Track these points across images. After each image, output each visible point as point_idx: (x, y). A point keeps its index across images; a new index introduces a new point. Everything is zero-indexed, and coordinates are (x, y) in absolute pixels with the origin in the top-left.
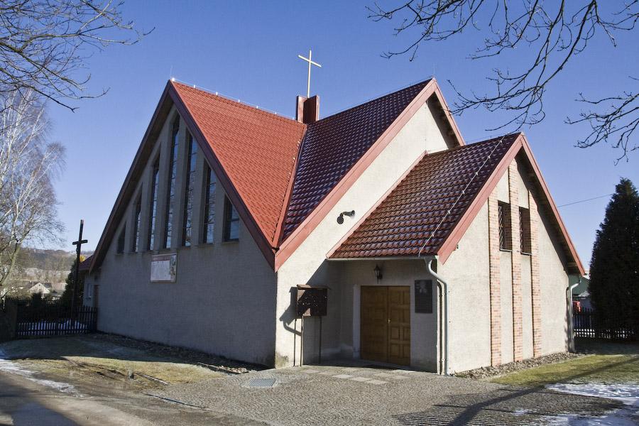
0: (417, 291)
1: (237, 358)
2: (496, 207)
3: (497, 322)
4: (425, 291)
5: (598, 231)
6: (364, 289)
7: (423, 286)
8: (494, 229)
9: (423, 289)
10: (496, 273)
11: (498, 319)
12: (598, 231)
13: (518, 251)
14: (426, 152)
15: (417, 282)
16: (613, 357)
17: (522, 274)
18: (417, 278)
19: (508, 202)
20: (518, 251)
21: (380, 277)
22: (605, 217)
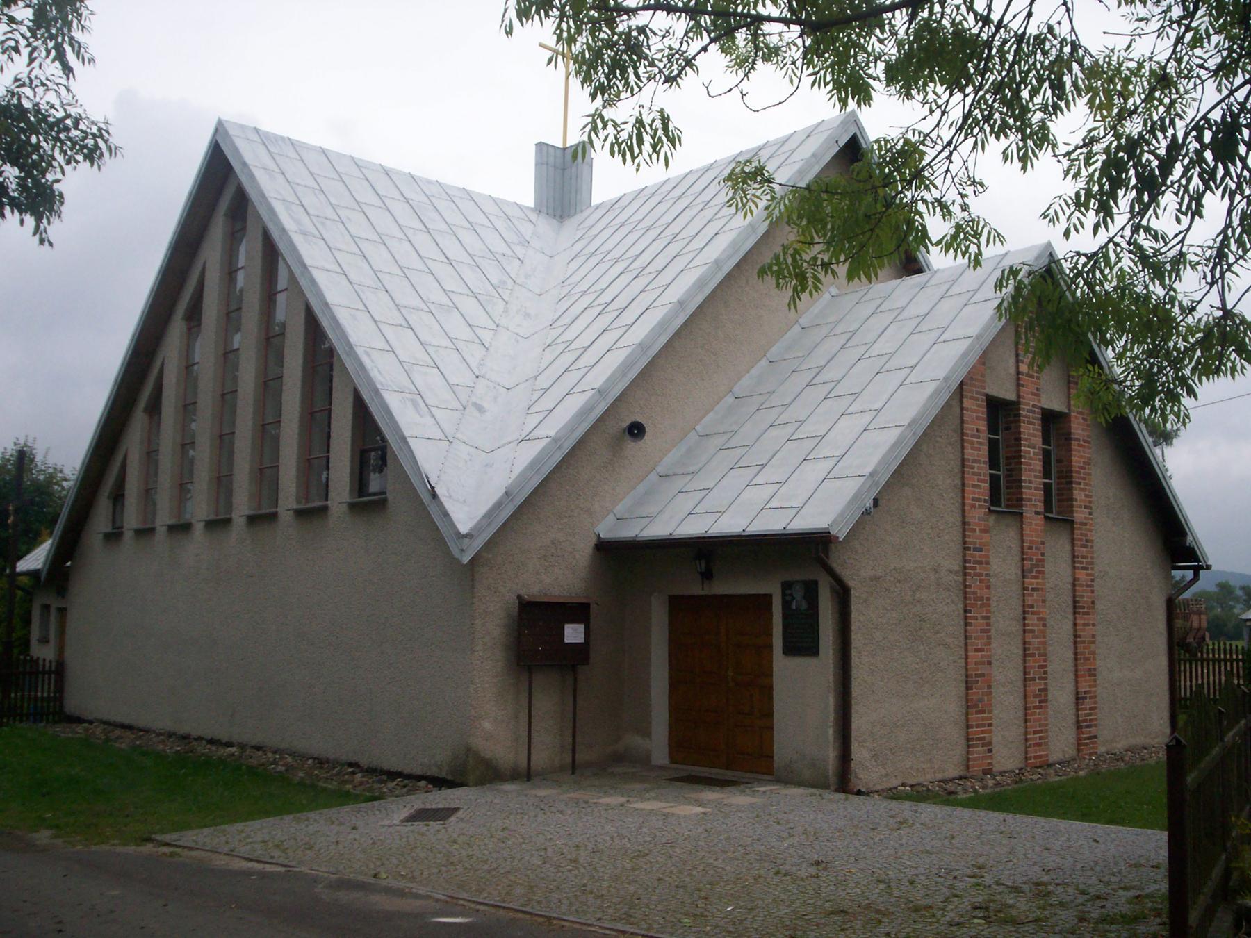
0: (786, 604)
1: (386, 766)
2: (982, 413)
3: (982, 675)
4: (804, 605)
5: (851, 276)
6: (677, 604)
7: (798, 593)
8: (975, 461)
9: (799, 603)
10: (980, 563)
11: (984, 669)
12: (851, 276)
13: (1037, 513)
14: (541, 146)
15: (787, 586)
16: (344, 896)
17: (1049, 568)
18: (788, 577)
19: (1011, 396)
20: (1037, 513)
21: (707, 576)
22: (770, 139)
